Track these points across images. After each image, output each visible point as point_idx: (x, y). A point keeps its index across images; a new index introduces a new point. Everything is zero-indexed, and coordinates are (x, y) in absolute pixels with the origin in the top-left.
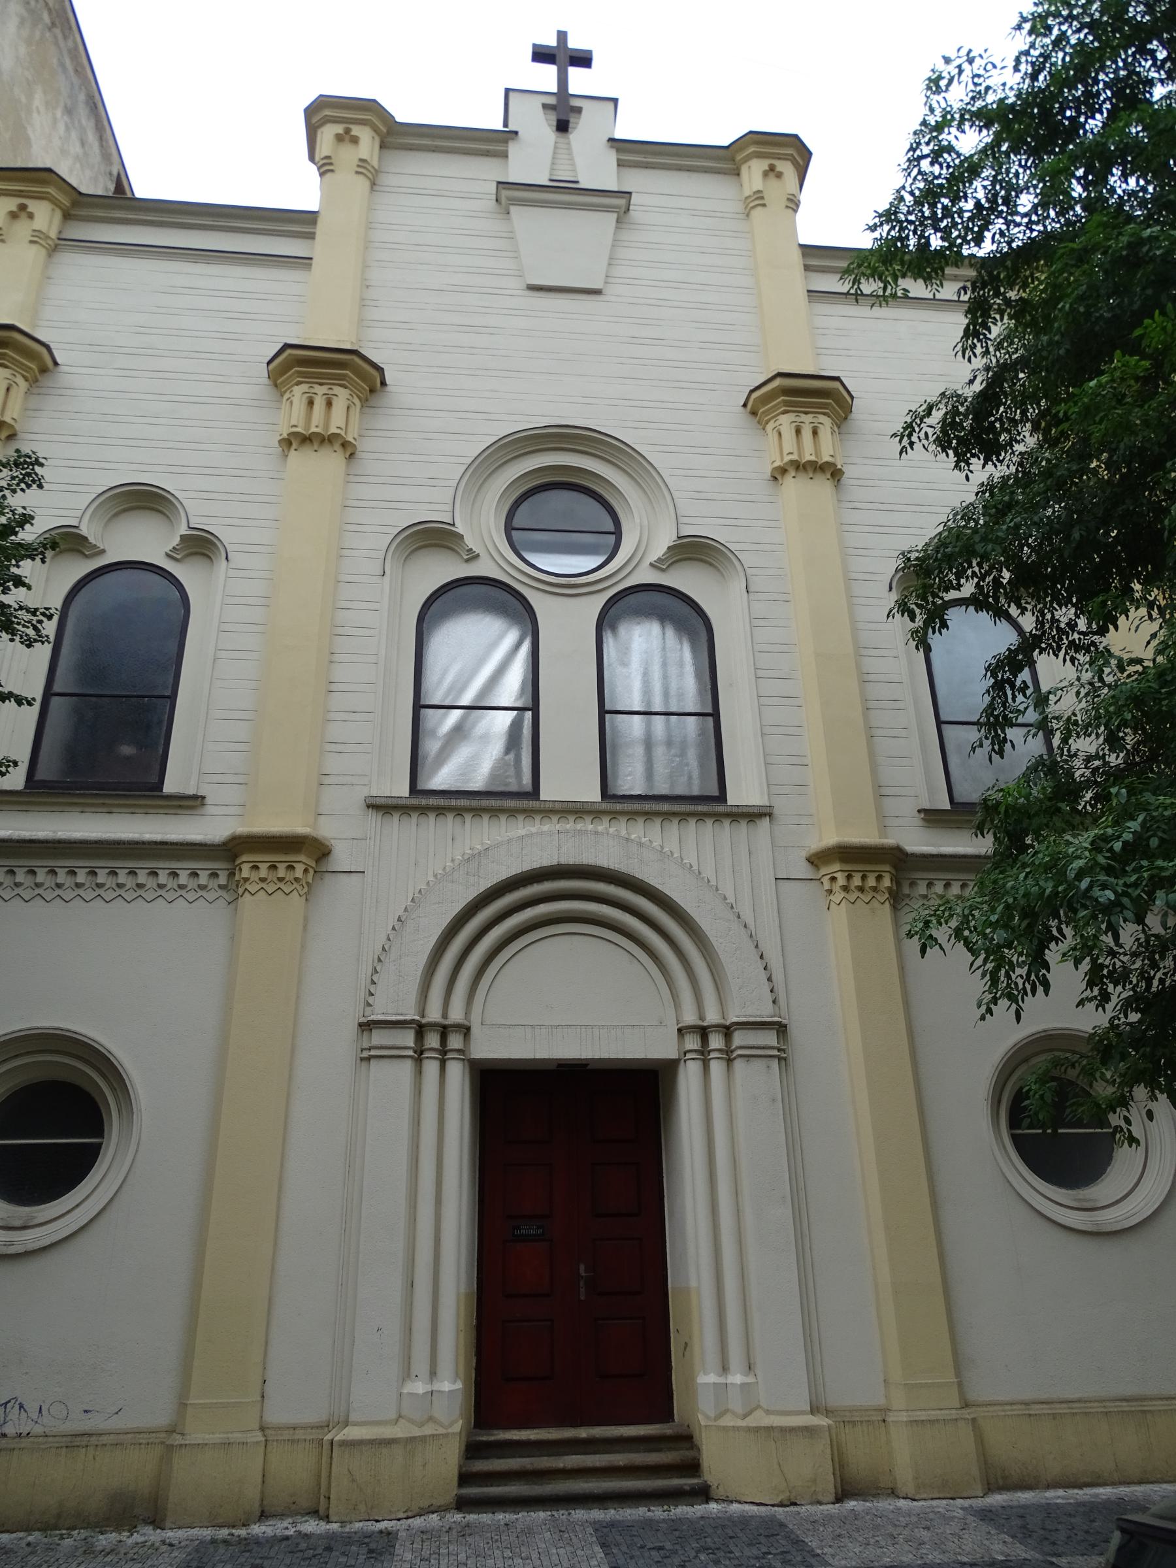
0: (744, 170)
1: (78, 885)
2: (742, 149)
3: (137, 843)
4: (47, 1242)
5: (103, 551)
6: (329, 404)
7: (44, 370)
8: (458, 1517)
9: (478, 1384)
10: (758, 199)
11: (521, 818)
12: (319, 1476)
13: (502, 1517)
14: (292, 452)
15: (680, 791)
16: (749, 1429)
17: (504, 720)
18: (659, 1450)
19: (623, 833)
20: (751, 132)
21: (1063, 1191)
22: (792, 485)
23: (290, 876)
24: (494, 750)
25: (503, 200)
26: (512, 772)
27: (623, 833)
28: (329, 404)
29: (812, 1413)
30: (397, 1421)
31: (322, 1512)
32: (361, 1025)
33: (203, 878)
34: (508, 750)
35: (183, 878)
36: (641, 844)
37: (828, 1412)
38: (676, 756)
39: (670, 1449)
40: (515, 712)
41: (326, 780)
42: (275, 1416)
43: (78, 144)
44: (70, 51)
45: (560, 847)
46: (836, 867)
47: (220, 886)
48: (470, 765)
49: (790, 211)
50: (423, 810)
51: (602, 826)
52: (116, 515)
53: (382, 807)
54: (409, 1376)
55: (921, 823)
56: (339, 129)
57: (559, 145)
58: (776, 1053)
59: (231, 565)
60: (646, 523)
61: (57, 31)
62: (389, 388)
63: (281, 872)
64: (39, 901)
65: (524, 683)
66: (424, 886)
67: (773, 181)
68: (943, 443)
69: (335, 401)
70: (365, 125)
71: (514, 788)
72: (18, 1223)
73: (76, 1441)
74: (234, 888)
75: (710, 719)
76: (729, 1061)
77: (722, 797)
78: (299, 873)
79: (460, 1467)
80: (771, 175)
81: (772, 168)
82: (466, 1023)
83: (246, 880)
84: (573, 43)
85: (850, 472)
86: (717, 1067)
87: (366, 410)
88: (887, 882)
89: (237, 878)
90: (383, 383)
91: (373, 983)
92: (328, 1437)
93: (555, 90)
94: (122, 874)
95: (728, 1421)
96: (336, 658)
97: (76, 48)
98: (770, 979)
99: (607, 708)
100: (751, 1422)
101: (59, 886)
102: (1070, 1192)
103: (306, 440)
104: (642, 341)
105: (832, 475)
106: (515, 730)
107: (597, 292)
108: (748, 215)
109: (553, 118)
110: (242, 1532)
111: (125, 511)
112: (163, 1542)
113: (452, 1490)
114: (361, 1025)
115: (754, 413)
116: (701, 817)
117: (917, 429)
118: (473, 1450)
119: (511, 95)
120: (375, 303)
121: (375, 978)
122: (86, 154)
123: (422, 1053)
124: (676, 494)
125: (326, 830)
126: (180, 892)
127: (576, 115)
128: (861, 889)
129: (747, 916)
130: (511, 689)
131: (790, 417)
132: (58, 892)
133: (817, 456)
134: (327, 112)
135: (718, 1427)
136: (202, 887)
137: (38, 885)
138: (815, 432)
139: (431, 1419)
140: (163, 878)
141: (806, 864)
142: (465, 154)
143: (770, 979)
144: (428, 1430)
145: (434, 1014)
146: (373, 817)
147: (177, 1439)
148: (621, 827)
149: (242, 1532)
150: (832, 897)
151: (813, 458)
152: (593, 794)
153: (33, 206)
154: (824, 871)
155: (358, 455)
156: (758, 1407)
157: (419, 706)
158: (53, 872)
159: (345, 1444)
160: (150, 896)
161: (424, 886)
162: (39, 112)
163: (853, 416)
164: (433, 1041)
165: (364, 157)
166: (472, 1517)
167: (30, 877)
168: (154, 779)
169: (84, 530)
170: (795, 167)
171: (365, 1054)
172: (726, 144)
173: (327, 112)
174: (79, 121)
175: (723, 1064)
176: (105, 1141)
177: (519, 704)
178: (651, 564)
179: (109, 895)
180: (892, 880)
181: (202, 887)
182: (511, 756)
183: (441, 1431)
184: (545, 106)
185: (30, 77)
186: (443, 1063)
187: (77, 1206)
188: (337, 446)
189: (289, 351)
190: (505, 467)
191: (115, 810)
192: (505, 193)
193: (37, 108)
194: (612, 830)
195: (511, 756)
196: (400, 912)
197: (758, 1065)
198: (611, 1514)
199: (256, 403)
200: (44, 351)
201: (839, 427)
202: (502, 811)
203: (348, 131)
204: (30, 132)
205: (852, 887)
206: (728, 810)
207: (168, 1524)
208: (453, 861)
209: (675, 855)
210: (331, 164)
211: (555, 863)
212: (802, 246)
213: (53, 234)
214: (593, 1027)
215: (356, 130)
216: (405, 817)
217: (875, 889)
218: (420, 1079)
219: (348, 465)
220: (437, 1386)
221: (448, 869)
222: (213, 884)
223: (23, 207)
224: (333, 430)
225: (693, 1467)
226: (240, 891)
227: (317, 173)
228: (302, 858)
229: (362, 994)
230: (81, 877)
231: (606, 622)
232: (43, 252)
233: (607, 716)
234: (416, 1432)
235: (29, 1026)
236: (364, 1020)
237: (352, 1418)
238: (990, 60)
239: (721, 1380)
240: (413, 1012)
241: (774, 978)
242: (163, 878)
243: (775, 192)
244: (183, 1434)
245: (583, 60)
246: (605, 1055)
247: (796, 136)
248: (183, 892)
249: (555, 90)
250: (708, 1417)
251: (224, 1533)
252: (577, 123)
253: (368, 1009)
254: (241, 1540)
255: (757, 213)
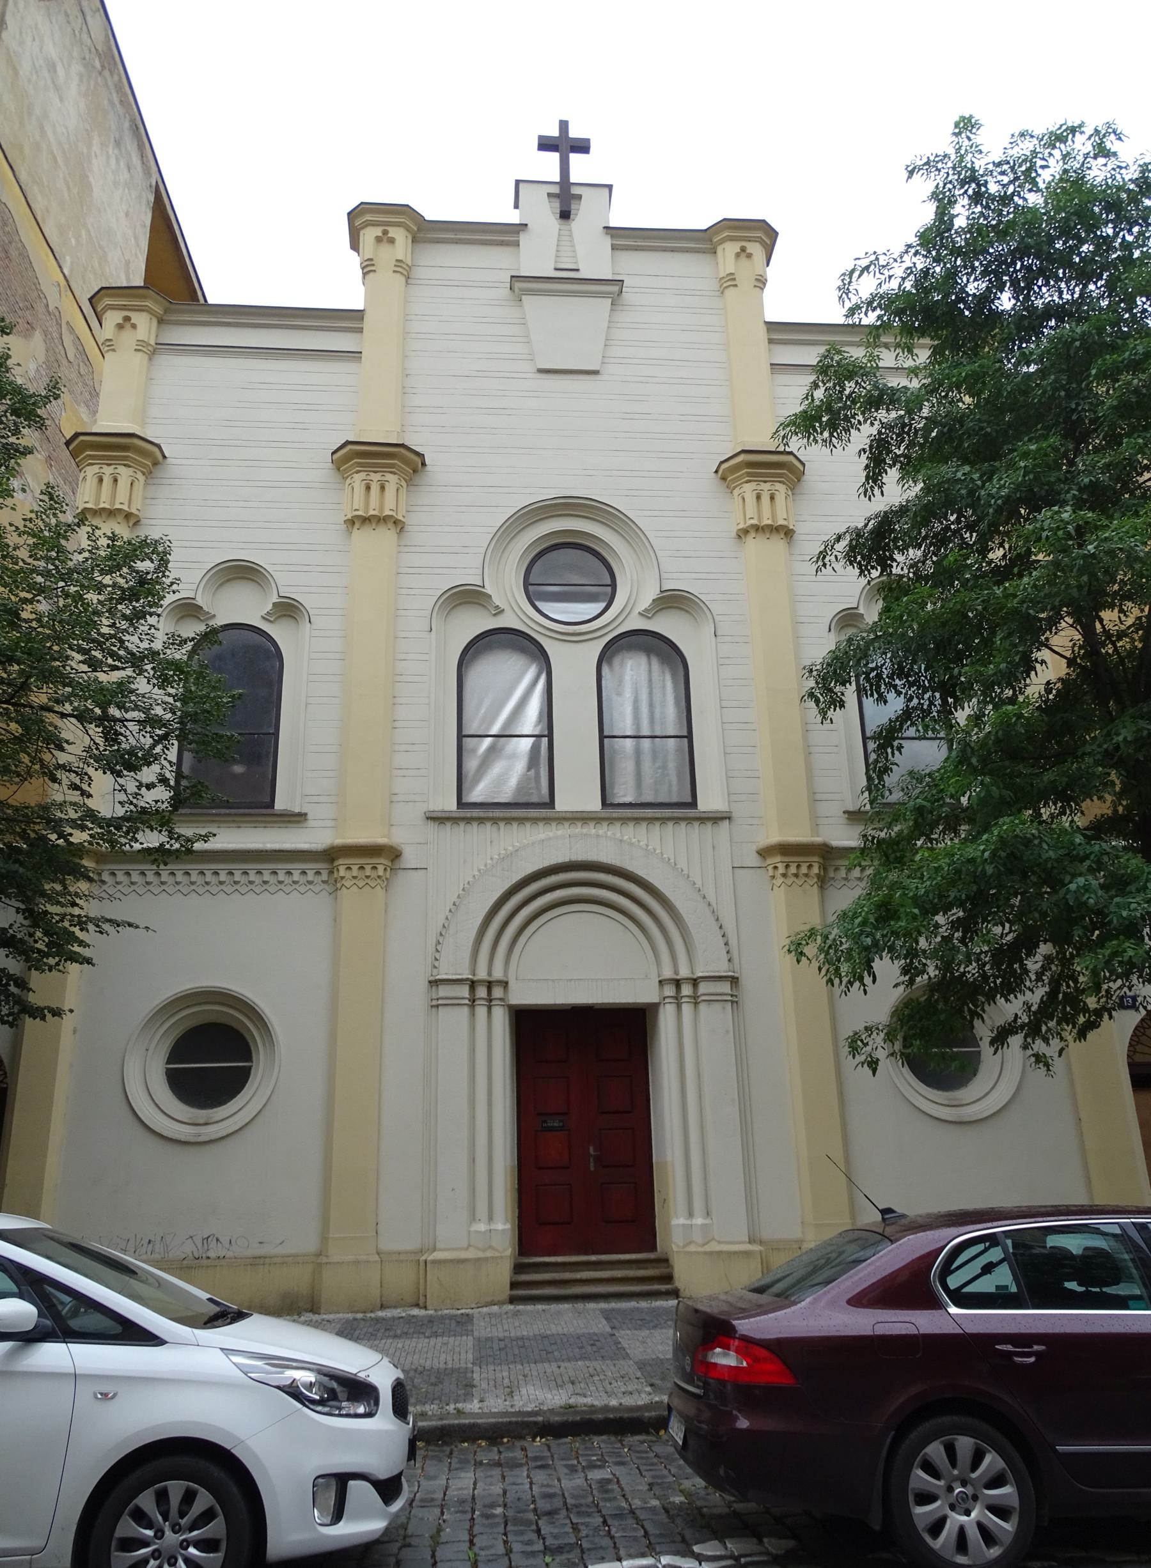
0: (719, 249)
1: (221, 883)
2: (717, 233)
3: (262, 851)
4: (224, 1133)
5: (214, 616)
6: (383, 488)
7: (156, 463)
8: (511, 1307)
9: (520, 1227)
10: (730, 281)
11: (541, 824)
12: (418, 1283)
13: (540, 1307)
14: (355, 531)
15: (662, 798)
16: (705, 1253)
17: (526, 744)
18: (646, 1268)
19: (618, 835)
20: (725, 220)
21: (940, 1093)
22: (753, 543)
23: (374, 874)
24: (520, 766)
25: (516, 290)
26: (533, 784)
27: (618, 835)
28: (383, 488)
29: (750, 1242)
30: (467, 1248)
31: (421, 1304)
32: (430, 982)
33: (310, 876)
34: (529, 769)
35: (296, 876)
36: (631, 844)
37: (761, 1243)
38: (659, 768)
39: (654, 1267)
40: (533, 739)
41: (395, 798)
42: (386, 1245)
43: (126, 170)
44: (116, 86)
45: (571, 849)
46: (778, 859)
47: (323, 882)
48: (501, 780)
49: (758, 289)
50: (469, 820)
51: (603, 829)
52: (221, 585)
53: (438, 819)
54: (474, 1219)
55: (845, 821)
56: (378, 231)
57: (562, 232)
58: (729, 998)
59: (314, 626)
60: (635, 577)
61: (106, 73)
62: (428, 468)
63: (368, 872)
64: (194, 895)
65: (541, 713)
66: (471, 879)
67: (744, 261)
68: (851, 561)
69: (387, 485)
70: (399, 226)
71: (535, 799)
72: (201, 1121)
73: (256, 1261)
74: (334, 884)
75: (686, 740)
76: (696, 1004)
77: (693, 804)
78: (381, 872)
79: (511, 1278)
80: (743, 255)
81: (743, 249)
82: (505, 979)
83: (342, 878)
84: (574, 133)
85: (410, 520)
86: (687, 1009)
87: (412, 488)
88: (816, 870)
89: (336, 875)
90: (424, 464)
91: (437, 951)
92: (423, 1258)
93: (558, 180)
94: (252, 873)
95: (692, 1248)
96: (398, 700)
97: (120, 80)
98: (726, 944)
99: (606, 733)
100: (707, 1248)
101: (207, 883)
102: (945, 1094)
103: (366, 520)
104: (631, 416)
105: (785, 534)
106: (535, 751)
107: (596, 372)
108: (722, 293)
109: (557, 205)
110: (373, 1315)
111: (228, 581)
112: (323, 1320)
113: (507, 1292)
114: (430, 982)
115: (724, 479)
116: (677, 820)
117: (830, 553)
118: (519, 1268)
119: (521, 185)
120: (414, 391)
121: (439, 948)
122: (132, 177)
123: (474, 1001)
124: (659, 554)
125: (397, 838)
126: (295, 886)
127: (577, 202)
128: (796, 876)
129: (711, 897)
130: (530, 720)
131: (753, 485)
132: (207, 888)
133: (773, 521)
134: (368, 217)
135: (686, 1253)
136: (310, 883)
137: (192, 883)
138: (772, 498)
139: (490, 1247)
140: (281, 876)
141: (755, 855)
142: (483, 244)
143: (726, 944)
144: (489, 1254)
145: (482, 974)
146: (432, 825)
147: (324, 1260)
148: (616, 830)
149: (373, 1315)
150: (774, 881)
151: (769, 522)
152: (595, 805)
153: (136, 318)
154: (769, 861)
155: (407, 528)
156: (713, 1239)
157: (461, 736)
158: (202, 873)
159: (434, 1262)
160: (273, 889)
161: (471, 879)
162: (96, 156)
163: (805, 478)
164: (482, 992)
165: (400, 258)
166: (521, 1307)
167: (186, 877)
168: (267, 799)
169: (200, 601)
170: (764, 247)
171: (434, 1003)
172: (705, 228)
173: (368, 217)
174: (126, 149)
175: (692, 1006)
176: (254, 1064)
177: (536, 733)
178: (639, 613)
179: (244, 889)
180: (819, 868)
181: (310, 883)
182: (532, 772)
183: (497, 1254)
184: (549, 195)
185: (89, 128)
186: (489, 1008)
187: (240, 1110)
188: (391, 525)
189: (350, 447)
190: (522, 533)
191: (242, 825)
192: (518, 285)
193: (95, 153)
194: (609, 833)
195: (532, 772)
196: (454, 898)
197: (717, 1007)
198: (613, 1305)
199: (322, 485)
200: (156, 450)
201: (791, 490)
202: (527, 819)
203: (385, 232)
204: (91, 179)
205: (789, 874)
206: (698, 815)
207: (322, 1311)
208: (492, 859)
209: (657, 852)
210: (373, 265)
211: (567, 860)
212: (767, 323)
213: (152, 342)
214: (597, 980)
215: (393, 232)
216: (455, 825)
217: (806, 875)
218: (474, 1019)
219: (398, 538)
220: (493, 1227)
221: (488, 866)
222: (318, 879)
223: (127, 319)
224: (387, 512)
225: (669, 1278)
226: (339, 885)
227: (360, 272)
228: (382, 861)
229: (430, 959)
230: (223, 876)
231: (605, 657)
232: (146, 357)
233: (606, 740)
234: (481, 1255)
235: (197, 985)
236: (432, 978)
237: (438, 1246)
238: (892, 256)
239: (688, 1222)
240: (467, 972)
241: (730, 943)
242: (281, 876)
243: (745, 272)
244: (327, 1256)
245: (582, 147)
246: (606, 1001)
247: (764, 221)
248: (296, 886)
249: (558, 180)
250: (678, 1246)
251: (359, 1316)
252: (578, 210)
253: (435, 971)
254: (372, 1319)
255: (730, 292)
